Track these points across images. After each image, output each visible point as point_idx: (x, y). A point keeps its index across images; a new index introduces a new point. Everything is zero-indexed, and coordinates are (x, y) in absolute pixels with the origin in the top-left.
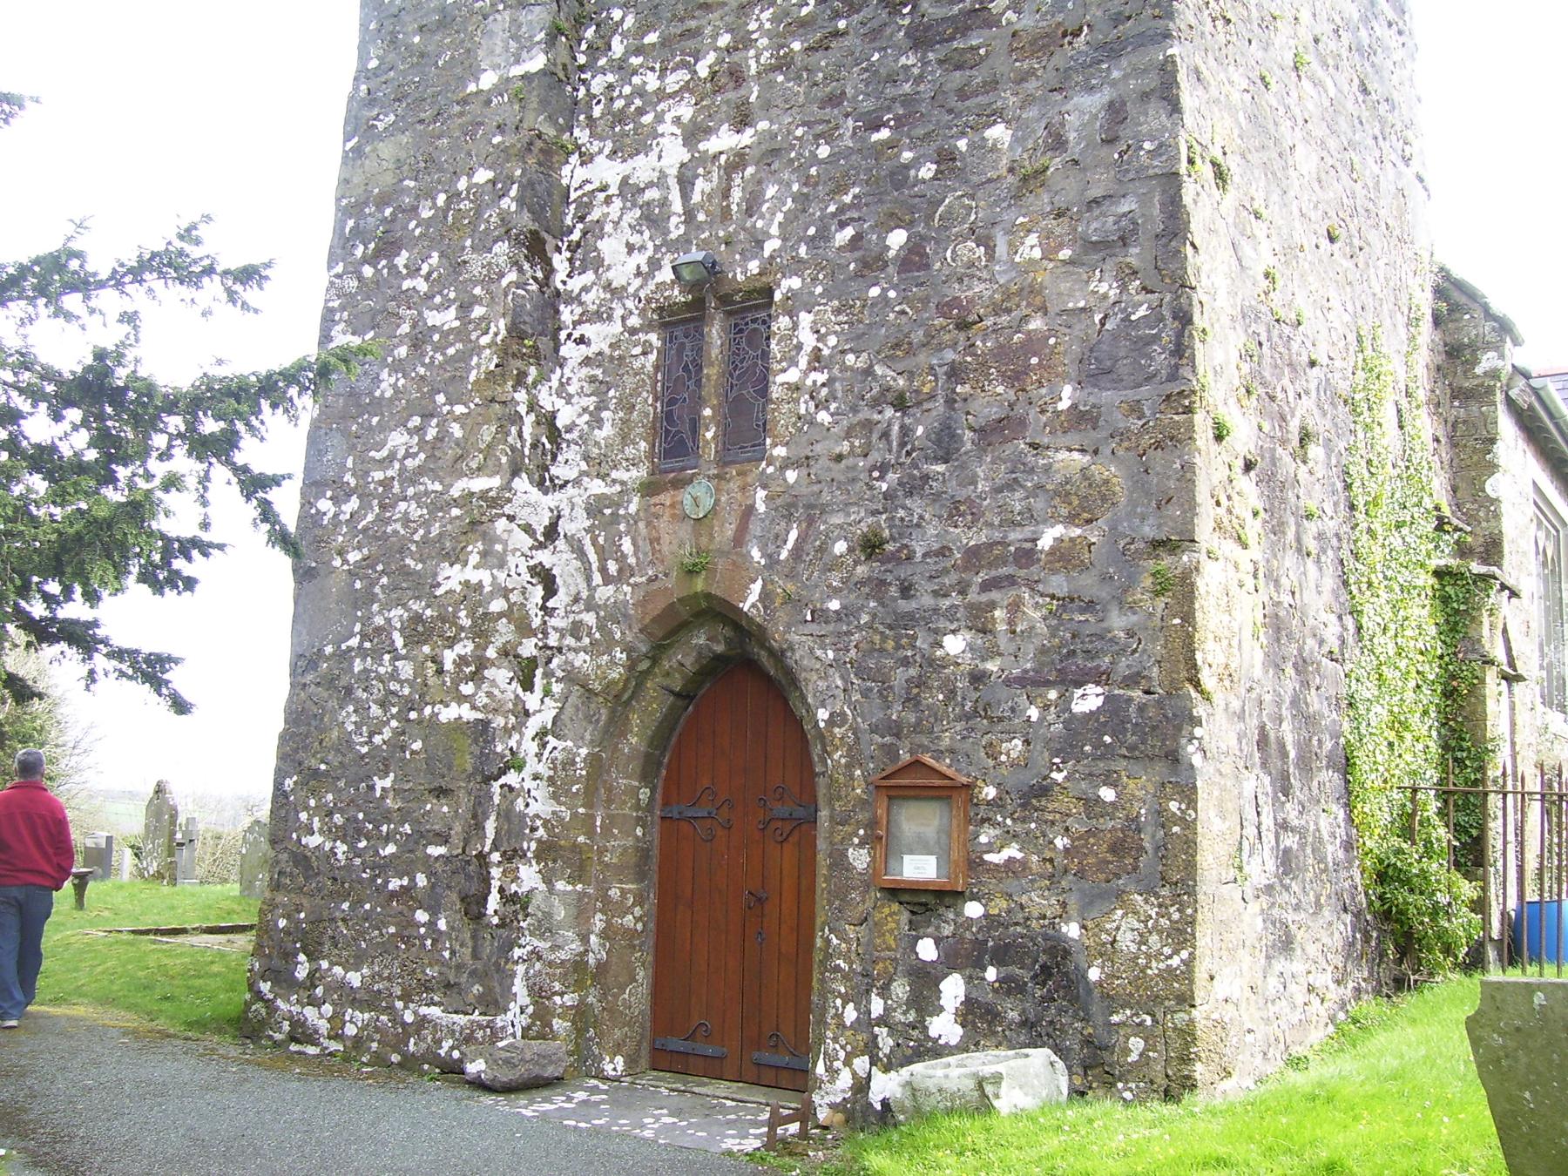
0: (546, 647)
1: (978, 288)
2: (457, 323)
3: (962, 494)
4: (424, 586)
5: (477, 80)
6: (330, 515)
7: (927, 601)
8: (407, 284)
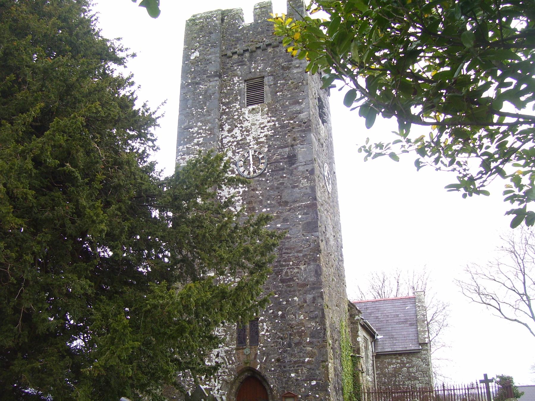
7: (288, 368)
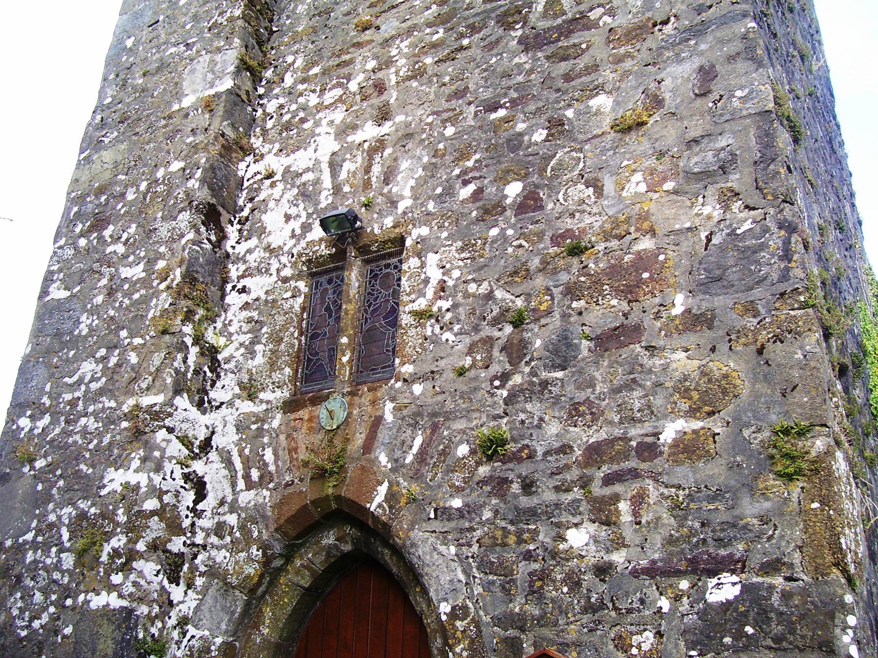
0: (194, 545)
1: (588, 220)
2: (143, 275)
3: (581, 396)
4: (89, 487)
5: (180, 101)
6: (27, 430)
7: (549, 496)
8: (109, 250)
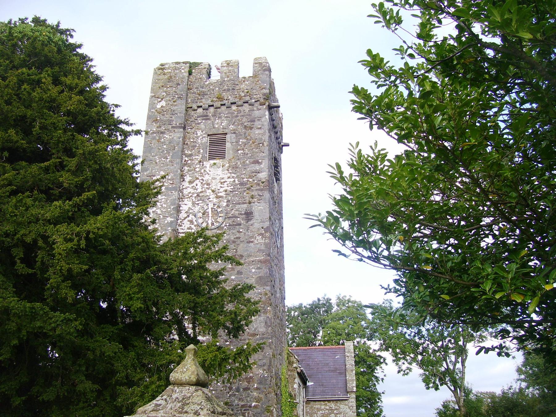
7: (236, 412)
